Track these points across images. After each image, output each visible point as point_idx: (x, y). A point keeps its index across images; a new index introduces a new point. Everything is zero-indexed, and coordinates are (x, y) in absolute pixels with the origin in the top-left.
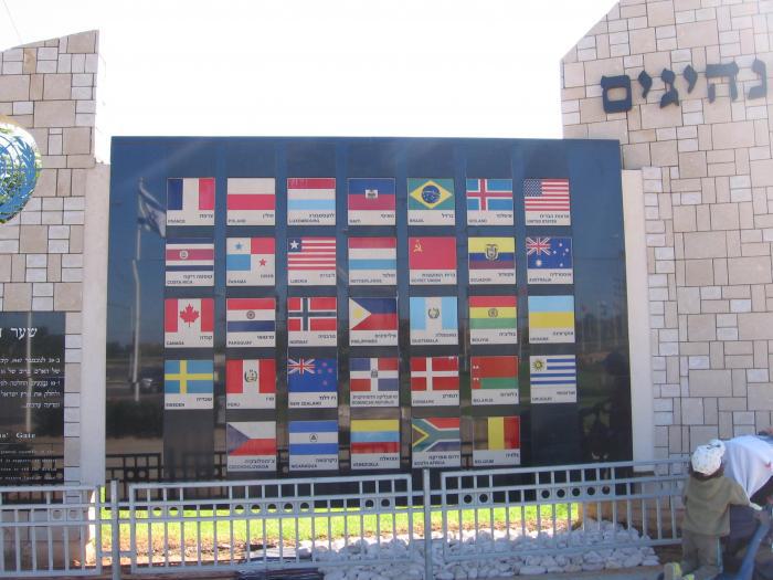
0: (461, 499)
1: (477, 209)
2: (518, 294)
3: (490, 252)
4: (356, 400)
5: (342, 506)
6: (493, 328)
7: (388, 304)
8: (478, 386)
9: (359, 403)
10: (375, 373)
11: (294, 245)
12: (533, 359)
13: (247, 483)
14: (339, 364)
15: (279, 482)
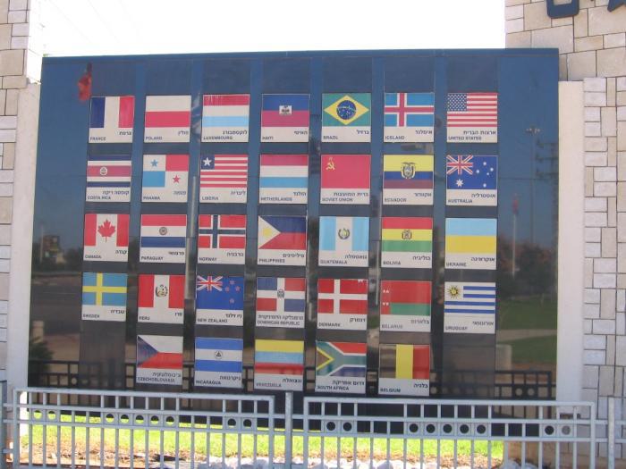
0: (324, 425)
1: (395, 125)
2: (434, 218)
3: (406, 171)
4: (262, 319)
5: (205, 423)
6: (407, 251)
7: (301, 224)
8: (387, 311)
9: (265, 322)
10: (281, 292)
11: (207, 162)
12: (448, 285)
13: (162, 395)
14: (244, 284)
15: (240, 398)
